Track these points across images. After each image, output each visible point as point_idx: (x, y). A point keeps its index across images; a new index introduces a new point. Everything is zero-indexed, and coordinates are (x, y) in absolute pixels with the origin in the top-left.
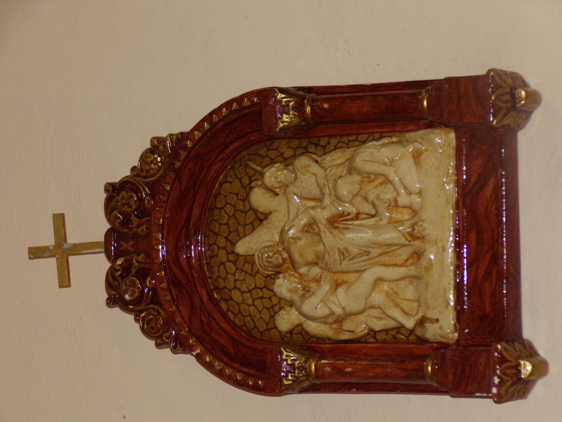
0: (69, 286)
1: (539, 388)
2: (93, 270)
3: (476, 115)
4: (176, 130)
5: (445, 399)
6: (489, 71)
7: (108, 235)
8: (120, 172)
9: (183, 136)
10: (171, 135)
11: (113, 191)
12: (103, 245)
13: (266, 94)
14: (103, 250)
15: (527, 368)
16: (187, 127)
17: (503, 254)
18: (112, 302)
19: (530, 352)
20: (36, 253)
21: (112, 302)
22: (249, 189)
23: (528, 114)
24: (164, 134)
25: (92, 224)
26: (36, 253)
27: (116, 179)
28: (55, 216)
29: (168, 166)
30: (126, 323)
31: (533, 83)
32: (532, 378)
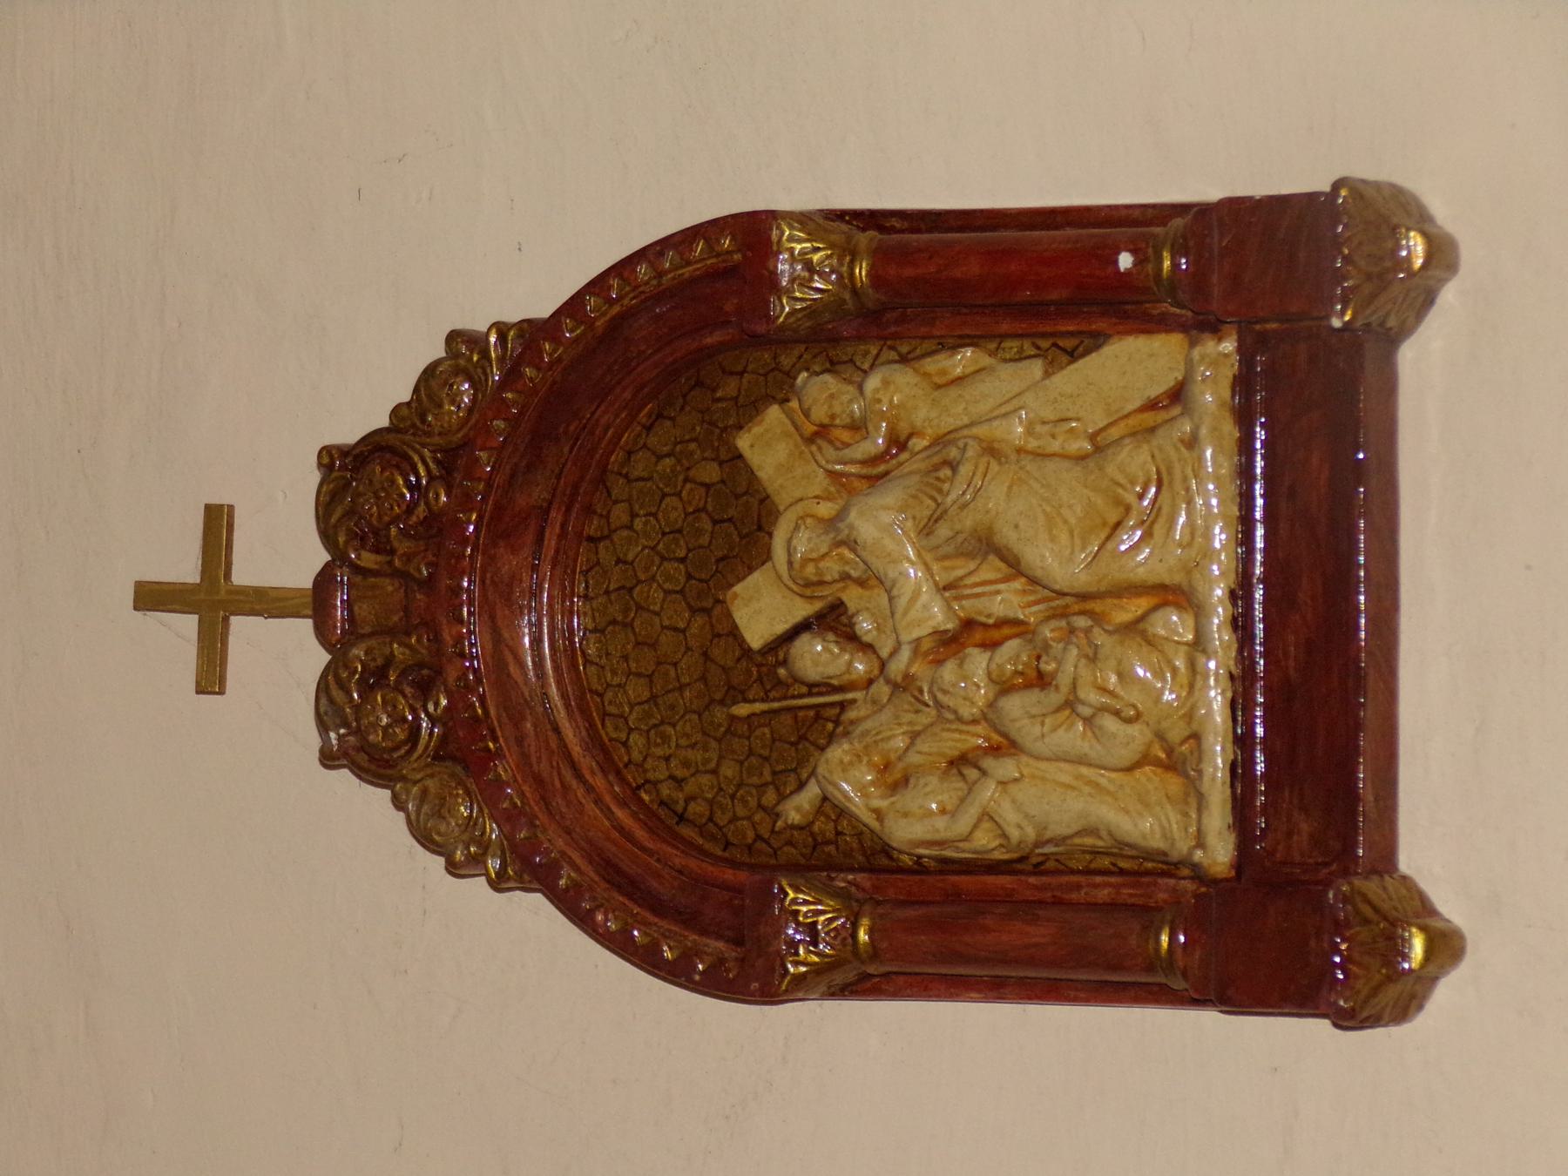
0: (222, 693)
1: (1446, 993)
2: (283, 661)
3: (1290, 306)
4: (513, 314)
5: (1210, 1019)
6: (1337, 186)
7: (324, 580)
8: (362, 412)
9: (532, 332)
10: (501, 329)
11: (346, 470)
12: (309, 599)
13: (753, 232)
14: (310, 612)
15: (1415, 247)
16: (543, 308)
17: (1358, 628)
18: (328, 759)
19: (1424, 910)
20: (151, 597)
21: (328, 759)
22: (750, 409)
23: (1429, 299)
24: (478, 322)
25: (284, 545)
26: (151, 597)
27: (349, 432)
28: (208, 508)
29: (488, 404)
30: (368, 811)
31: (1442, 212)
32: (1431, 968)
